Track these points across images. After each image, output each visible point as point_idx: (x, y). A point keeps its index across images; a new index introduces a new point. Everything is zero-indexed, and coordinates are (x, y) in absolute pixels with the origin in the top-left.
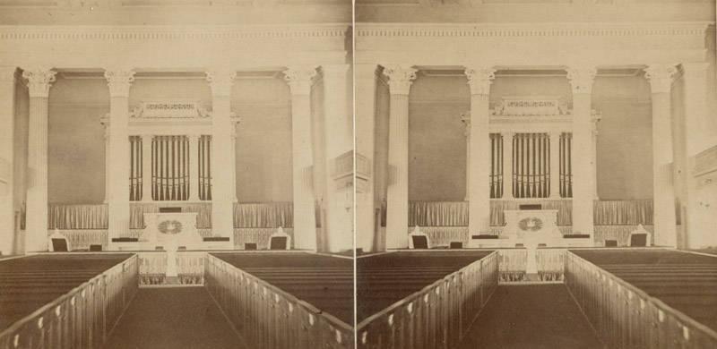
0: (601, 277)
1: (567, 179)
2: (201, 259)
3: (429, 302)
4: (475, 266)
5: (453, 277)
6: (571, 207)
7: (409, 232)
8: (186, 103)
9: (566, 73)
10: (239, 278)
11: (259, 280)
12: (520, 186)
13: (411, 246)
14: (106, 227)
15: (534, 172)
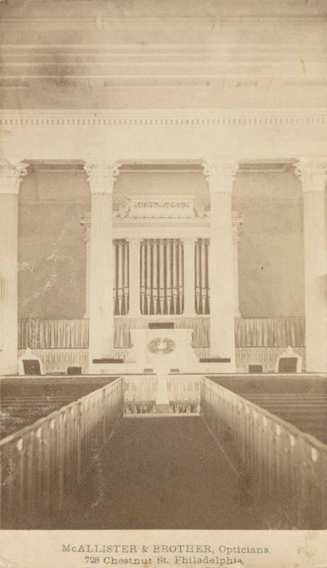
0: (244, 408)
1: (204, 292)
2: (196, 384)
3: (42, 437)
4: (96, 396)
5: (70, 408)
6: (209, 327)
7: (18, 356)
8: (180, 201)
9: (203, 168)
10: (238, 406)
11: (259, 409)
12: (149, 300)
13: (22, 372)
14: (86, 346)
15: (165, 285)
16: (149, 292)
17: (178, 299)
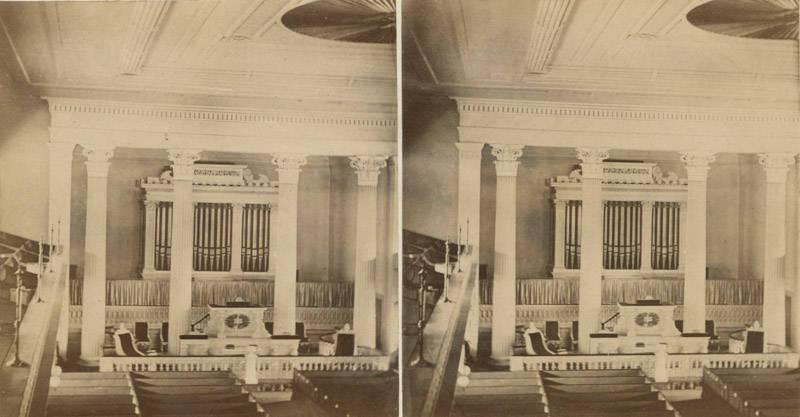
16: (610, 249)
17: (226, 257)
